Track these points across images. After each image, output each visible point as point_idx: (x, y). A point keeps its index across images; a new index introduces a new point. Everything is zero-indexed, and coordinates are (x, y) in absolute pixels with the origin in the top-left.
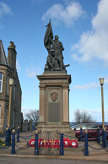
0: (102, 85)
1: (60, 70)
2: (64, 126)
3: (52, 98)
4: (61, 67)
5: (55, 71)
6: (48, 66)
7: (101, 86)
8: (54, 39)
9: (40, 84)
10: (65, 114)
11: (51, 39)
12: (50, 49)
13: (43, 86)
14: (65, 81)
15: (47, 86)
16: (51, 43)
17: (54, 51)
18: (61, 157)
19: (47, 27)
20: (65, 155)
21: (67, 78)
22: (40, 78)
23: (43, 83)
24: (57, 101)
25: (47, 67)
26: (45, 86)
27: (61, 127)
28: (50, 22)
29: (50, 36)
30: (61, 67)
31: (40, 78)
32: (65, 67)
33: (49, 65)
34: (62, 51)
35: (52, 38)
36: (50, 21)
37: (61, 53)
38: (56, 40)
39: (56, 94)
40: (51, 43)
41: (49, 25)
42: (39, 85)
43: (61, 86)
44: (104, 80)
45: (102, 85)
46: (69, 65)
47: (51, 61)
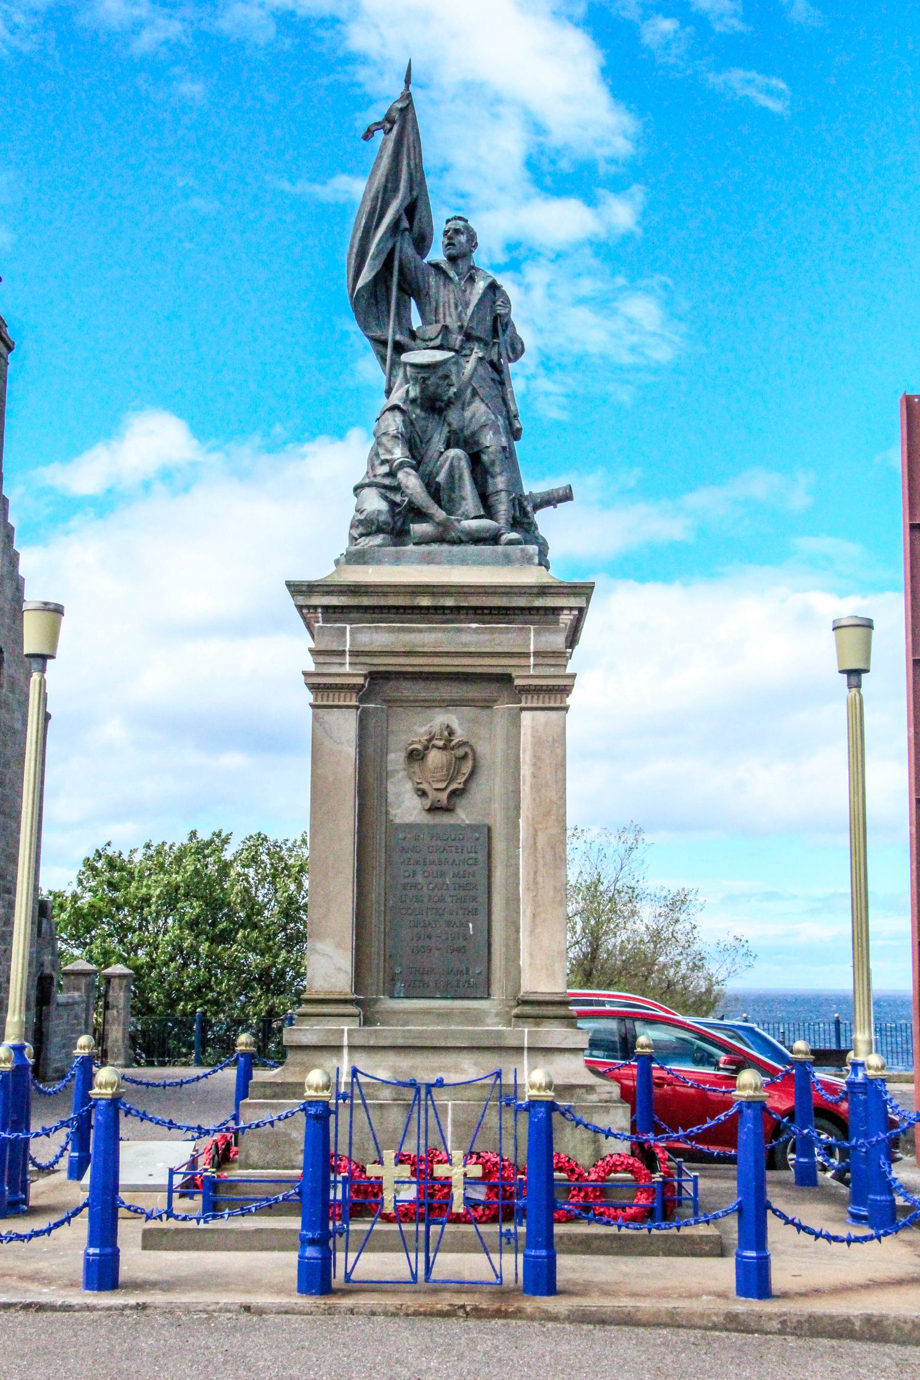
0: (854, 675)
1: (494, 539)
2: (525, 1034)
3: (424, 786)
4: (503, 507)
5: (445, 547)
6: (386, 498)
7: (850, 686)
8: (437, 254)
9: (321, 659)
10: (534, 926)
11: (409, 250)
12: (399, 348)
13: (339, 681)
14: (543, 639)
15: (376, 677)
16: (411, 288)
17: (444, 362)
18: (531, 1304)
19: (379, 135)
20: (784, 1295)
21: (556, 611)
22: (325, 605)
23: (342, 653)
24: (463, 815)
25: (375, 503)
26: (360, 681)
27: (436, 1043)
28: (407, 97)
29: (405, 224)
30: (503, 507)
31: (325, 605)
32: (536, 507)
33: (397, 489)
34: (510, 360)
35: (422, 243)
36: (408, 81)
37: (502, 383)
38: (452, 259)
39: (460, 752)
40: (411, 288)
41: (402, 121)
42: (312, 668)
43: (505, 679)
44: (65, 620)
45: (854, 675)
46: (567, 496)
47: (413, 457)
